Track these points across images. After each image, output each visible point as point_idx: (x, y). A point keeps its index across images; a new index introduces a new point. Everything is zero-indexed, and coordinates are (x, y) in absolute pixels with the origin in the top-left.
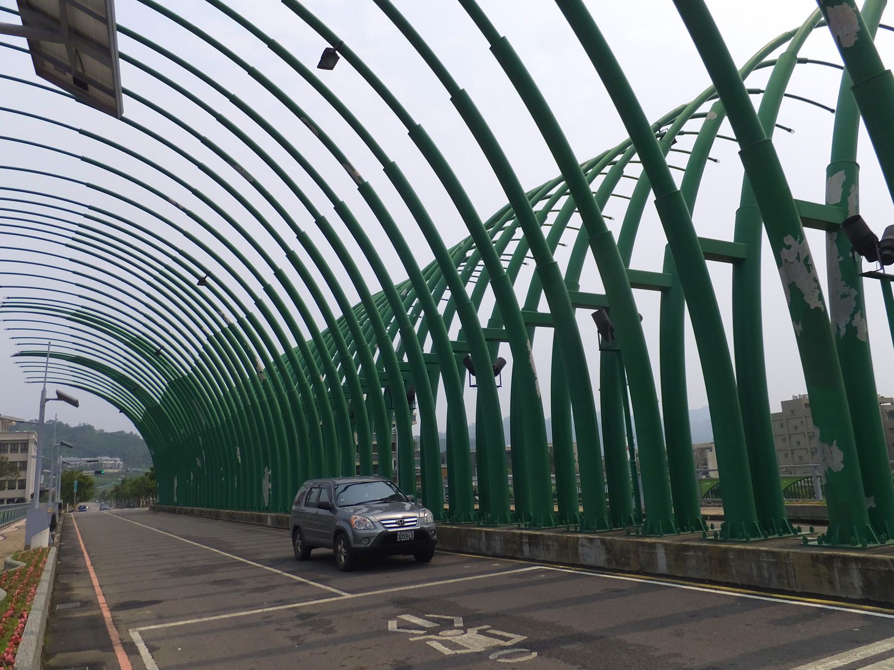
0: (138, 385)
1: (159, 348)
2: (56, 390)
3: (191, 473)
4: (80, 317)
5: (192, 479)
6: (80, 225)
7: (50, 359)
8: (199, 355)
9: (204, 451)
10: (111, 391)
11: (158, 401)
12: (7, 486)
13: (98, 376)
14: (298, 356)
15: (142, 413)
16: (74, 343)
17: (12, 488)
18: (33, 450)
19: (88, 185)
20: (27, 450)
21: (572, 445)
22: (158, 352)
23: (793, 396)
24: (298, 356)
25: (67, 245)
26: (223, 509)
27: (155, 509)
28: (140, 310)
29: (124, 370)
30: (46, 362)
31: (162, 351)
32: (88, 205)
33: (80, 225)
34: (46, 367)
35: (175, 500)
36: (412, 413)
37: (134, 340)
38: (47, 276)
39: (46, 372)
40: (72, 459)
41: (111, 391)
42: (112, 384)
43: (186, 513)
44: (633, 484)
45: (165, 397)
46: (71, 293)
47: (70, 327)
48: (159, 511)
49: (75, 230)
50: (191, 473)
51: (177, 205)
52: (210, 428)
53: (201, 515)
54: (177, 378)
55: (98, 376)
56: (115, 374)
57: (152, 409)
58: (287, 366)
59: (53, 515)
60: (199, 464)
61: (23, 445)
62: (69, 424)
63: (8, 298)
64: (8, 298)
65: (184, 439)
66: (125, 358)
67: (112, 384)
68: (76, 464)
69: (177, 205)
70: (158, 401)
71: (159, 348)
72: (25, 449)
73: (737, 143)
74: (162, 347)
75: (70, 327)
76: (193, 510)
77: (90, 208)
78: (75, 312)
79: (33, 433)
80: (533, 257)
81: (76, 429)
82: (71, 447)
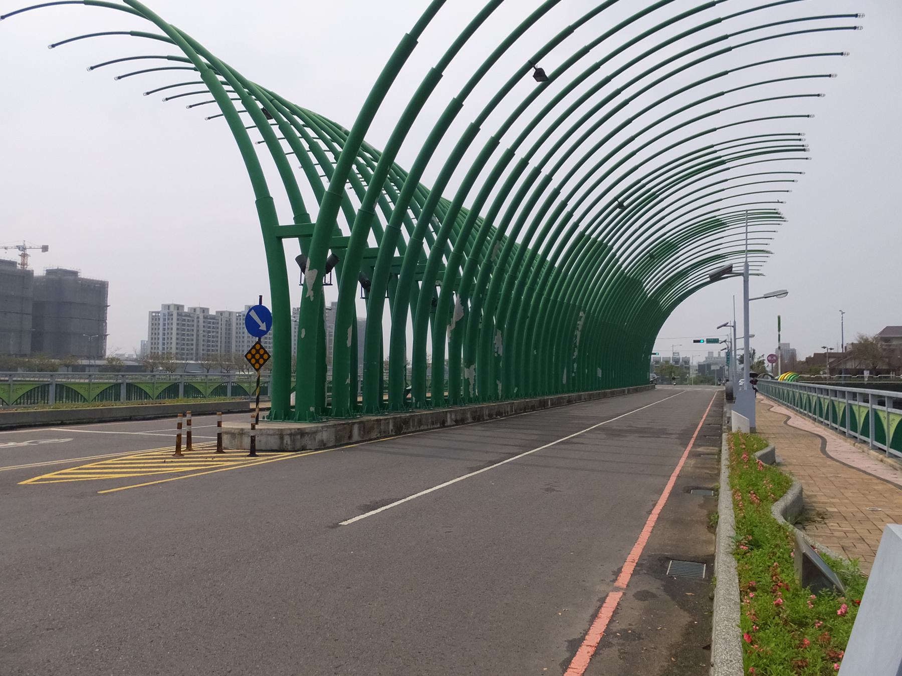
7: (745, 249)
13: (694, 259)
14: (528, 255)
15: (637, 277)
21: (274, 341)
24: (528, 255)
30: (748, 246)
34: (747, 239)
36: (573, 353)
38: (757, 118)
39: (747, 239)
44: (460, 388)
46: (728, 187)
47: (726, 180)
53: (591, 398)
55: (694, 259)
58: (536, 263)
59: (188, 432)
63: (779, 224)
64: (779, 224)
73: (205, 84)
75: (726, 180)
80: (284, 137)
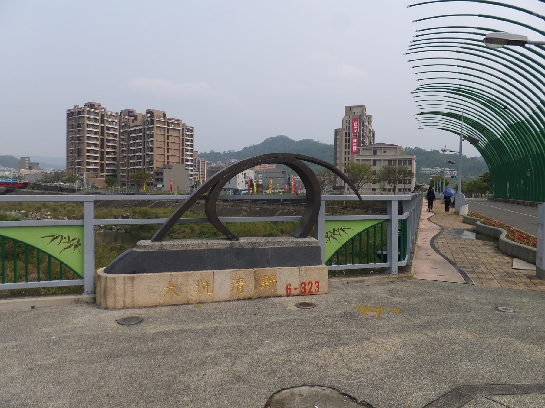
0: (486, 127)
1: (505, 104)
2: (78, 105)
3: (522, 180)
4: (458, 91)
5: (522, 184)
6: (469, 39)
8: (537, 107)
9: (533, 167)
10: (465, 131)
11: (499, 137)
12: (407, 182)
16: (449, 106)
17: (405, 183)
18: (414, 163)
19: (480, 16)
20: (411, 164)
22: (506, 107)
23: (442, 204)
25: (457, 52)
26: (165, 240)
27: (491, 199)
28: (496, 83)
29: (478, 119)
31: (508, 106)
32: (477, 27)
33: (469, 39)
35: (508, 195)
37: (489, 101)
40: (428, 169)
41: (465, 131)
42: (467, 127)
43: (518, 203)
45: (504, 134)
47: (448, 97)
48: (495, 201)
49: (464, 42)
50: (522, 180)
51: (538, 16)
52: (539, 152)
54: (515, 121)
56: (471, 121)
57: (494, 142)
60: (528, 174)
61: (404, 162)
62: (426, 149)
64: (421, 85)
65: (516, 159)
66: (479, 112)
67: (467, 127)
68: (430, 172)
69: (538, 16)
70: (499, 137)
71: (505, 104)
72: (411, 164)
74: (508, 104)
75: (448, 97)
76: (525, 202)
77: (479, 28)
78: (455, 88)
79: (414, 155)
81: (429, 152)
82: (454, 163)
